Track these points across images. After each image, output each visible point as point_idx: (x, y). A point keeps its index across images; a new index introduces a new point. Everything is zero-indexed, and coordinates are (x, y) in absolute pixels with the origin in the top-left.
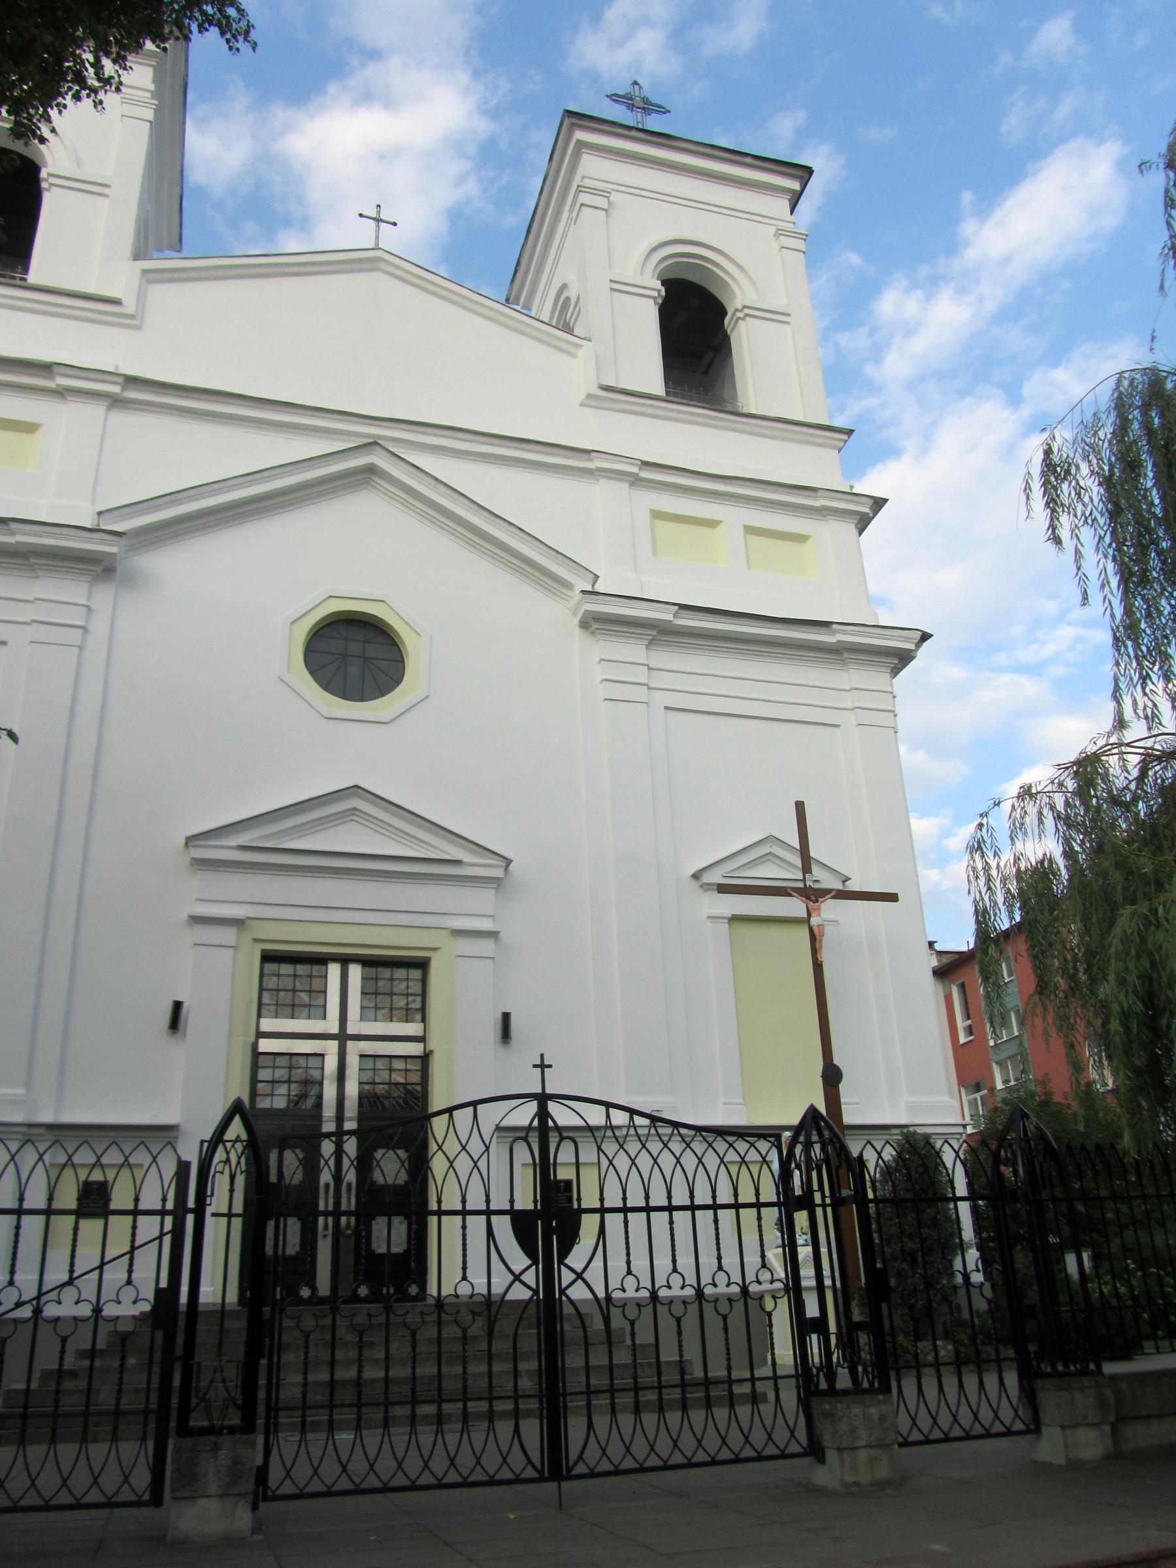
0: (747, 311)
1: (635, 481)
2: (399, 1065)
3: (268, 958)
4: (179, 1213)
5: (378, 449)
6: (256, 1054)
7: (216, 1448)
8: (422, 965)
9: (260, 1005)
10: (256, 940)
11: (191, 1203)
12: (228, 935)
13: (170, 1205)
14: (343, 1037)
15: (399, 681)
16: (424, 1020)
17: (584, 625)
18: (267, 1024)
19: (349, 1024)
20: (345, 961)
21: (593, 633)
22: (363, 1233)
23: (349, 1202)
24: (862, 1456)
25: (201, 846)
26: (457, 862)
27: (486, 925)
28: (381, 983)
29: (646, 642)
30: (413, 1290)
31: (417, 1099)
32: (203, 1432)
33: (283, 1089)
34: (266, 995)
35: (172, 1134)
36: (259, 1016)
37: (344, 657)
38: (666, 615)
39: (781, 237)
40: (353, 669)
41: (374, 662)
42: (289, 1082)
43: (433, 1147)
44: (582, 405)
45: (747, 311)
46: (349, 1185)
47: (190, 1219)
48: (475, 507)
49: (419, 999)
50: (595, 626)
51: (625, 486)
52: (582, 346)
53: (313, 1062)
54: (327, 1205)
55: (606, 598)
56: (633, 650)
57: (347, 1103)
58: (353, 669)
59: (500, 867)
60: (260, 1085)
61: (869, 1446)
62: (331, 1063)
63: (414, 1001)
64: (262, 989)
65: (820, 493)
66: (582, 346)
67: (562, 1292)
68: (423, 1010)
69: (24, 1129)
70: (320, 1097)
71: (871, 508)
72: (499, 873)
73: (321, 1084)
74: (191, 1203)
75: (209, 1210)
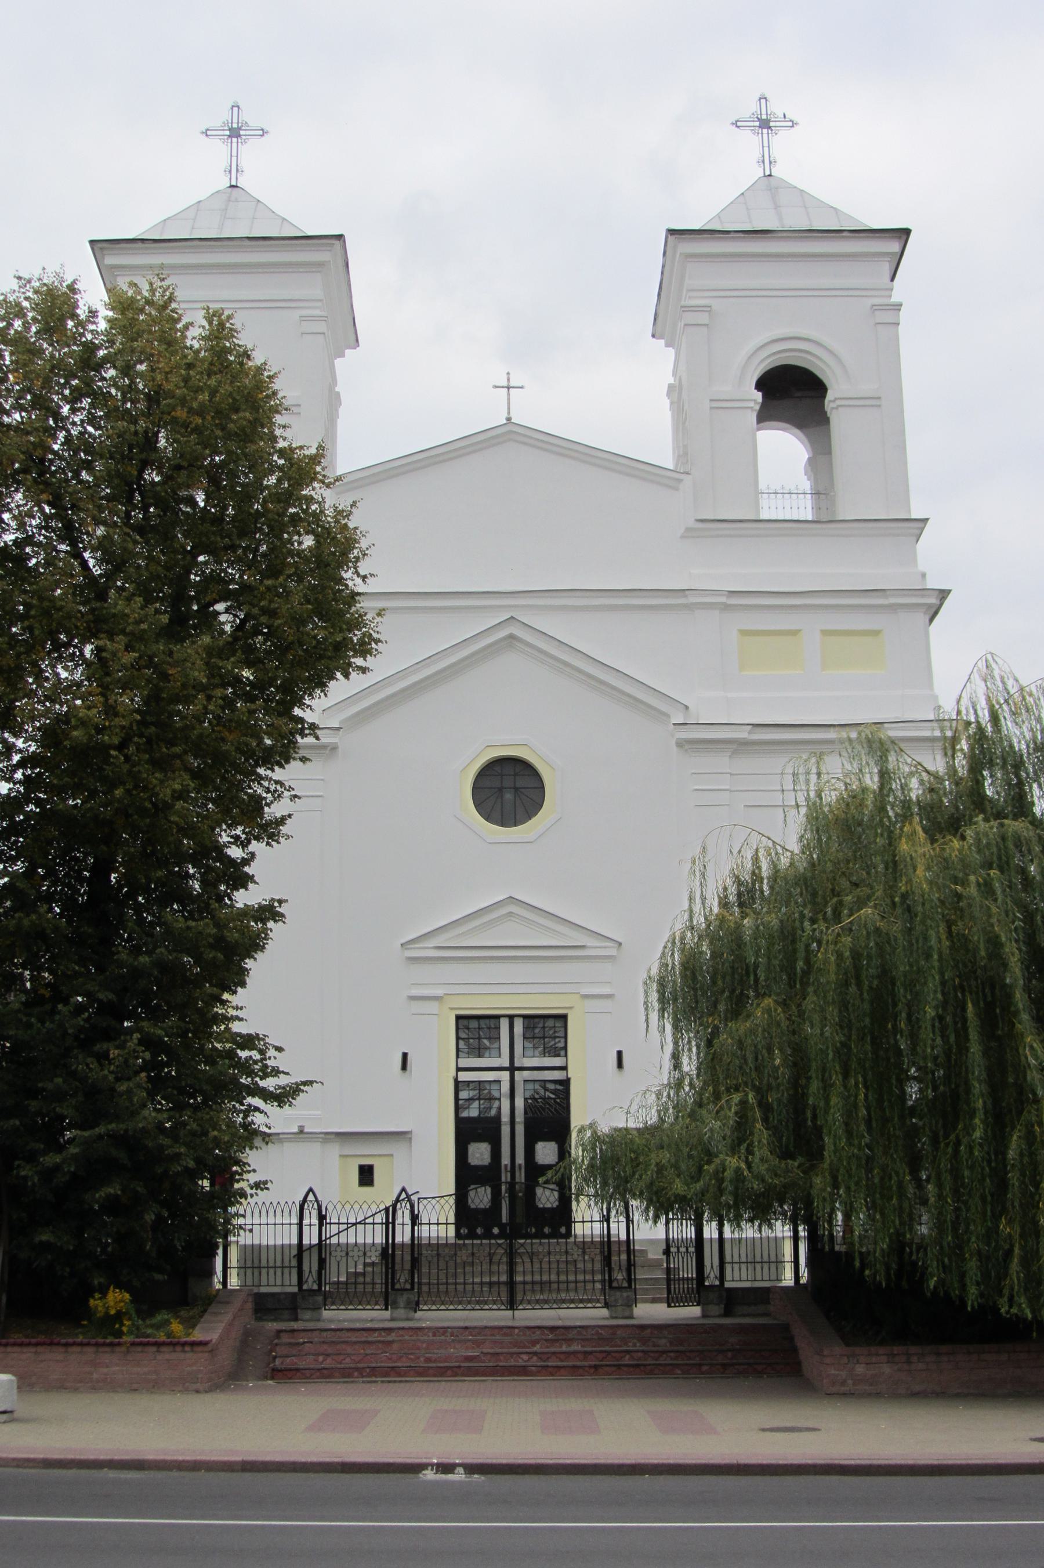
0: (839, 403)
1: (726, 608)
2: (551, 1086)
3: (459, 1018)
4: (387, 1223)
5: (514, 621)
6: (457, 1083)
7: (402, 1294)
8: (564, 1018)
9: (458, 1050)
10: (452, 1009)
11: (390, 1221)
12: (433, 1007)
13: (384, 1221)
14: (512, 1069)
15: (539, 805)
16: (566, 1055)
17: (680, 744)
18: (464, 1063)
19: (516, 1060)
20: (511, 1018)
21: (686, 750)
22: (530, 1194)
23: (521, 1177)
24: (620, 1309)
25: (411, 948)
26: (583, 947)
27: (606, 990)
28: (537, 1031)
29: (729, 754)
30: (563, 1230)
31: (563, 1108)
32: (398, 1290)
33: (476, 1104)
34: (461, 1042)
35: (409, 1136)
36: (458, 1056)
37: (501, 790)
38: (743, 734)
39: (877, 313)
40: (508, 796)
41: (523, 790)
42: (479, 1099)
43: (454, 1207)
44: (683, 537)
45: (839, 403)
46: (520, 1165)
47: (390, 1225)
48: (591, 660)
49: (563, 1040)
50: (686, 747)
51: (717, 612)
52: (682, 480)
53: (495, 1087)
54: (506, 1177)
55: (692, 726)
56: (722, 762)
57: (517, 1112)
58: (508, 796)
59: (613, 947)
60: (461, 1102)
61: (622, 1305)
62: (505, 1087)
63: (559, 1042)
64: (458, 1038)
65: (888, 593)
66: (682, 480)
67: (516, 1250)
68: (565, 1048)
69: (322, 1136)
70: (500, 1108)
71: (937, 598)
72: (613, 952)
73: (500, 1099)
74: (390, 1221)
75: (397, 1222)
